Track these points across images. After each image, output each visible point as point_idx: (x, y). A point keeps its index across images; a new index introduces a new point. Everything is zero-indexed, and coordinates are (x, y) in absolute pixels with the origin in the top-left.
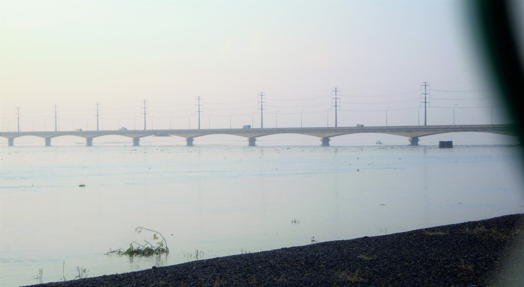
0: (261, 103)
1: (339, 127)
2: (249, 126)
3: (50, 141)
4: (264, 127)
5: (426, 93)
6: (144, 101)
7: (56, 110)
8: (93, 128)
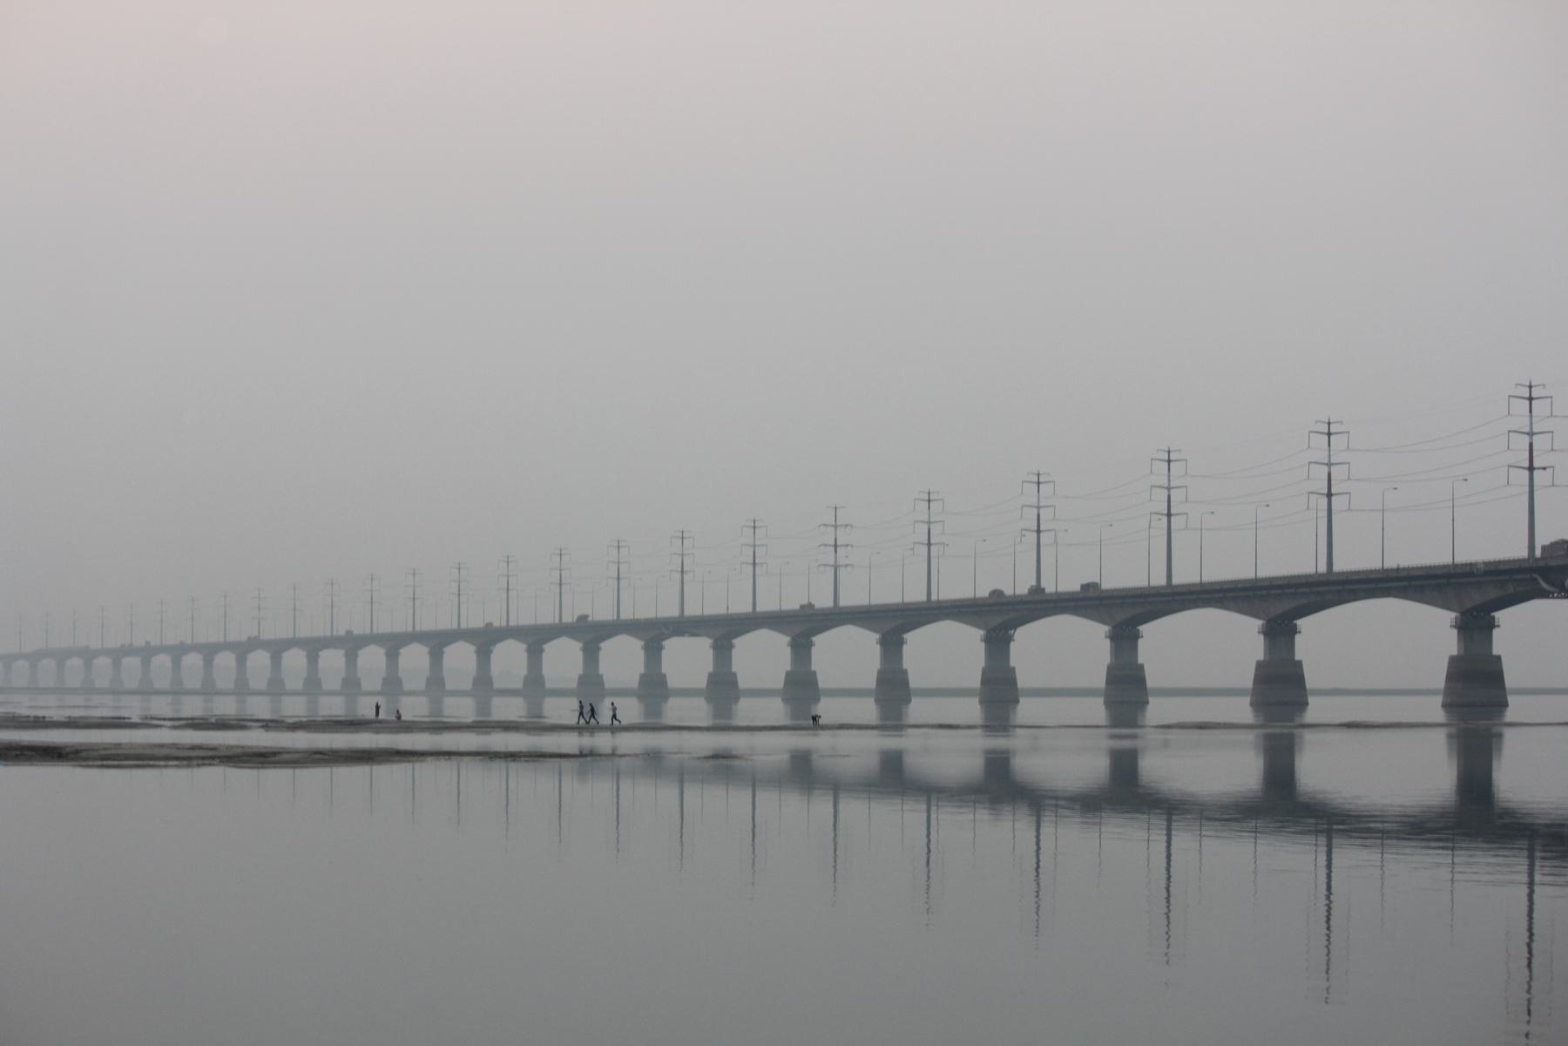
0: (1166, 491)
1: (1180, 586)
2: (586, 617)
3: (810, 649)
4: (758, 609)
5: (1535, 430)
6: (617, 544)
7: (1531, 424)
8: (1302, 562)
